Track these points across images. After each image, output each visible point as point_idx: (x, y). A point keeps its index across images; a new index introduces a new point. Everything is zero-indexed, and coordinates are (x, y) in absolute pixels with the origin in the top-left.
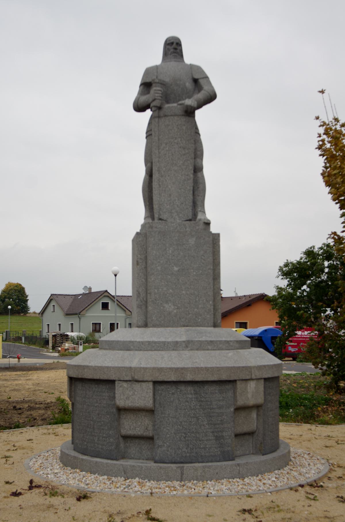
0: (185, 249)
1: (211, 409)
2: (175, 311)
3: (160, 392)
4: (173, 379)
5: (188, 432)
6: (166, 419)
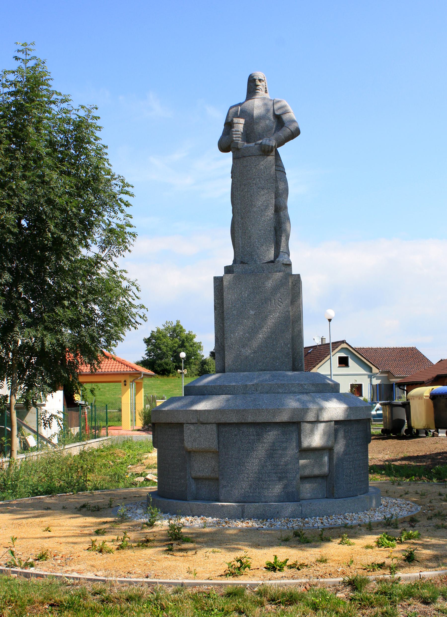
0: (261, 292)
1: (273, 451)
2: (252, 355)
3: (223, 434)
4: (234, 420)
5: (251, 473)
6: (230, 459)
